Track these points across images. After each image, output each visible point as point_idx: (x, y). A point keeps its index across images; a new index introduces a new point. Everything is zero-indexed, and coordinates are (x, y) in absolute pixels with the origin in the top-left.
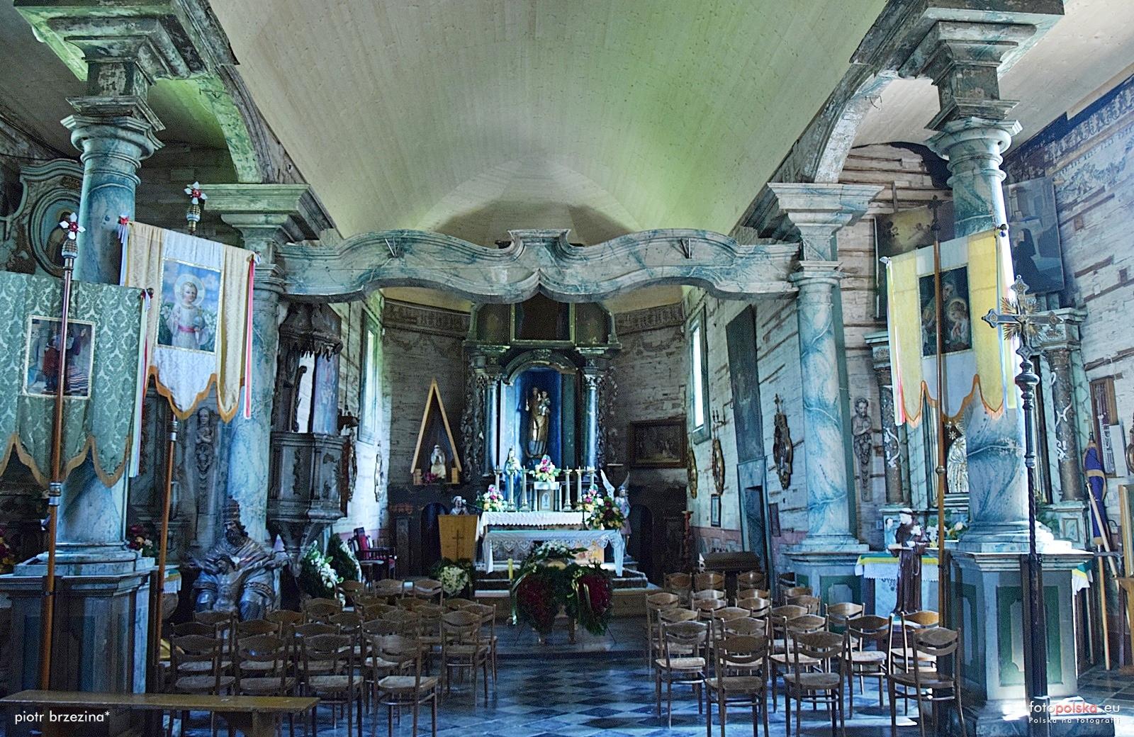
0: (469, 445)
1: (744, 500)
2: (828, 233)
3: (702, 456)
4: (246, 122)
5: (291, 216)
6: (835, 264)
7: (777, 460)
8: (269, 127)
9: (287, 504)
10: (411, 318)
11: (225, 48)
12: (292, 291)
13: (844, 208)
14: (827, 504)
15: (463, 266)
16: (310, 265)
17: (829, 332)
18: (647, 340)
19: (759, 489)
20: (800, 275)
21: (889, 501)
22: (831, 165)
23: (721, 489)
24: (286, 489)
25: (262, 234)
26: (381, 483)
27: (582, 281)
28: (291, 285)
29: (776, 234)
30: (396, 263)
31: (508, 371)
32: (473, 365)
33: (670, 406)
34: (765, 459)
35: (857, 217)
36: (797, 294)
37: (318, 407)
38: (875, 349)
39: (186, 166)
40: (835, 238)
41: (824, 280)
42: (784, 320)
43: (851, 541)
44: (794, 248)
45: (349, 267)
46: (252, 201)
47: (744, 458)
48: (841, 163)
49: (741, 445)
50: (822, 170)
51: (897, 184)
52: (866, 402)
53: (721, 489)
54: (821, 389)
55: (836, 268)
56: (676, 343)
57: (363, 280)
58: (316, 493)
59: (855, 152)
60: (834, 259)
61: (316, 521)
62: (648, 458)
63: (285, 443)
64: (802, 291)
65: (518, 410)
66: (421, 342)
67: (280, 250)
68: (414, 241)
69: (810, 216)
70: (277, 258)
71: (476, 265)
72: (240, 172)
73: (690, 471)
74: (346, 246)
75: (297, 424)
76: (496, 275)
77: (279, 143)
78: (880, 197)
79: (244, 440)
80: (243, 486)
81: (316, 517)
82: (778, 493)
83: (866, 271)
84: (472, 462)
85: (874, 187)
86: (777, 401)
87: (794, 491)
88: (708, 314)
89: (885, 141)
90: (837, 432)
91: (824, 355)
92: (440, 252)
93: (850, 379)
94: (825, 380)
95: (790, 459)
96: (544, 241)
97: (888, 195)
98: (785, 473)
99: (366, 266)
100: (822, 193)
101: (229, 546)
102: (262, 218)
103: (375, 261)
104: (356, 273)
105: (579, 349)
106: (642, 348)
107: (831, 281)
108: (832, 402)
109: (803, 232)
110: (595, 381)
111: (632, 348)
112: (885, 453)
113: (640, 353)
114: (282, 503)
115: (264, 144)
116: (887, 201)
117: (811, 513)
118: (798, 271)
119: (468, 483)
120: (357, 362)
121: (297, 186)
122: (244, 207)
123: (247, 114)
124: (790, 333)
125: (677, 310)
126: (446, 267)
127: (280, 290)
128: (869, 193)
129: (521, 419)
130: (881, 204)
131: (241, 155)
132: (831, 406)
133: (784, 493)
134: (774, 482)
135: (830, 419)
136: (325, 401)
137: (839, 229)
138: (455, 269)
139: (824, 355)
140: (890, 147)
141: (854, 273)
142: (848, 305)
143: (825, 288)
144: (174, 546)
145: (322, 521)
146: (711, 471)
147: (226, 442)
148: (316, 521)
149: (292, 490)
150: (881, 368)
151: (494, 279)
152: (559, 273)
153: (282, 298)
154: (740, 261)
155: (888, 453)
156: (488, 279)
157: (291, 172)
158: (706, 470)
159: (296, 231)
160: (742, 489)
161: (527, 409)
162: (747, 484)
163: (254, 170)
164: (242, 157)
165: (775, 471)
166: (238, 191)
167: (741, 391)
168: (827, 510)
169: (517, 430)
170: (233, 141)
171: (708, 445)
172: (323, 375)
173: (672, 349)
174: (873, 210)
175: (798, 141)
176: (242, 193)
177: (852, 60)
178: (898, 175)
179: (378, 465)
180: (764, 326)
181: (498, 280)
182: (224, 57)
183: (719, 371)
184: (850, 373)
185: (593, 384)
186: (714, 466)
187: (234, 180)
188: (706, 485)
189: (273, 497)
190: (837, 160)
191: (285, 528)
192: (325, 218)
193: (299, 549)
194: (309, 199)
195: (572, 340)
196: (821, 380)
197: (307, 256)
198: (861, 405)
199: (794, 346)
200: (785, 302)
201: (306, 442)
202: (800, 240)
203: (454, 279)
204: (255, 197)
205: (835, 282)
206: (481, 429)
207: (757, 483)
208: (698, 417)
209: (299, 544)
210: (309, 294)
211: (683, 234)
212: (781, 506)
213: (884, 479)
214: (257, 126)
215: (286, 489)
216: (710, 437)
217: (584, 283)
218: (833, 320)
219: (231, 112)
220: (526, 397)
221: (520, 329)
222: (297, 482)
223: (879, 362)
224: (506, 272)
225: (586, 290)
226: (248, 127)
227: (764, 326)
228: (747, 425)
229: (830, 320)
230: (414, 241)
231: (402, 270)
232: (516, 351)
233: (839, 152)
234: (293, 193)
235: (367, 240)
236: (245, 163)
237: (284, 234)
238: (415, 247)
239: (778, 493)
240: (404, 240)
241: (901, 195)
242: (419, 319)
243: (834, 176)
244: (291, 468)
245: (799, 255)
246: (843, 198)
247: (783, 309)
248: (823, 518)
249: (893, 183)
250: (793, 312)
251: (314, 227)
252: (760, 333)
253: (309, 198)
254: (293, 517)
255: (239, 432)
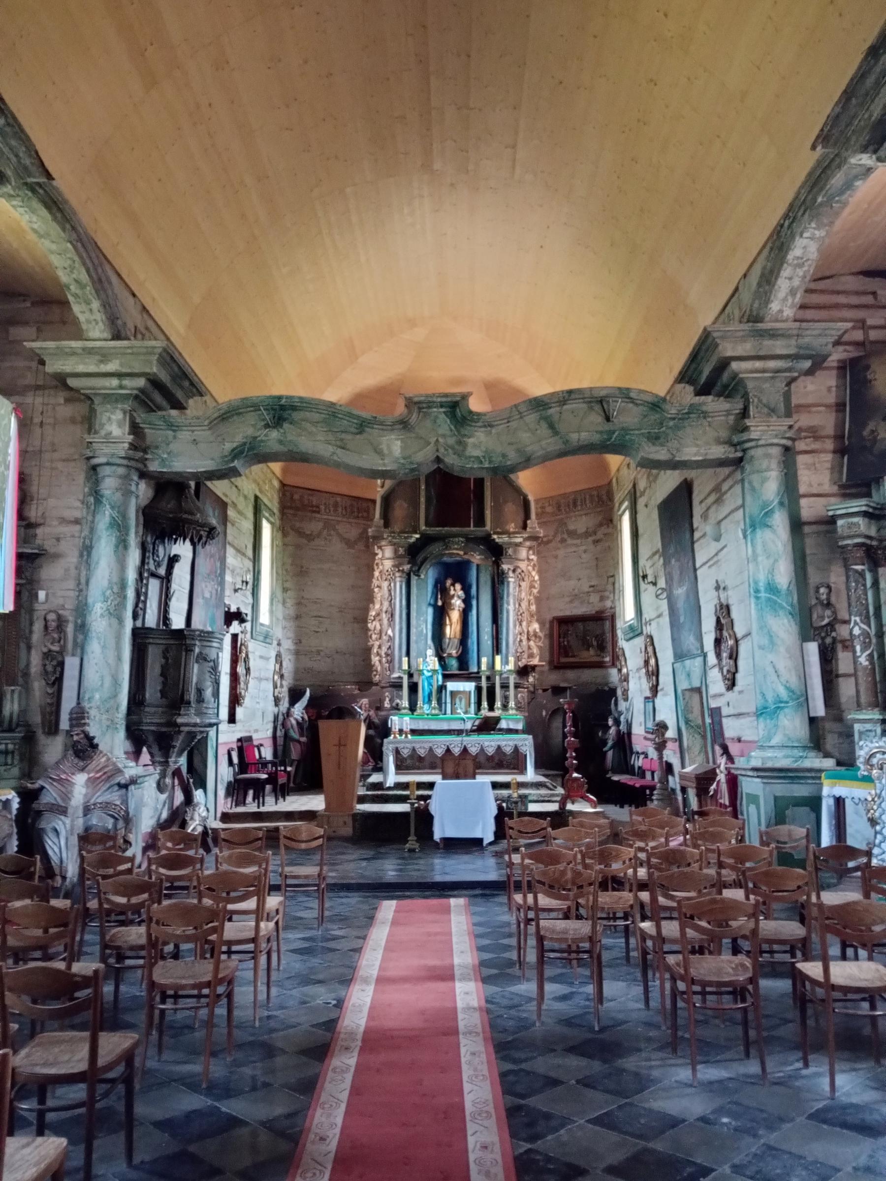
0: (377, 643)
1: (681, 702)
2: (781, 385)
3: (632, 652)
4: (84, 264)
5: (149, 380)
6: (789, 422)
7: (718, 655)
8: (119, 275)
9: (153, 710)
10: (312, 506)
11: (30, 156)
12: (154, 467)
13: (802, 352)
14: (782, 708)
15: (349, 437)
16: (175, 437)
17: (781, 504)
18: (572, 527)
19: (698, 690)
20: (745, 436)
21: (859, 706)
22: (785, 299)
23: (655, 690)
24: (152, 692)
25: (117, 401)
26: (282, 686)
27: (486, 452)
28: (152, 460)
29: (718, 388)
30: (274, 434)
31: (419, 562)
32: (380, 556)
33: (598, 598)
34: (705, 656)
35: (818, 363)
36: (741, 460)
37: (198, 601)
38: (840, 522)
39: (26, 323)
40: (789, 391)
41: (776, 441)
42: (726, 492)
43: (812, 754)
44: (738, 406)
45: (220, 439)
46: (101, 362)
47: (680, 656)
48: (798, 296)
49: (675, 641)
50: (775, 306)
51: (870, 322)
52: (829, 587)
53: (655, 690)
54: (772, 571)
55: (791, 427)
56: (604, 530)
57: (236, 454)
58: (186, 697)
59: (813, 286)
60: (788, 414)
61: (186, 729)
62: (573, 656)
63: (151, 641)
64: (748, 456)
65: (430, 604)
66: (325, 532)
67: (138, 420)
68: (294, 408)
69: (758, 364)
70: (135, 429)
71: (365, 435)
72: (84, 327)
73: (620, 670)
74: (216, 415)
75: (169, 619)
76: (389, 447)
77: (134, 295)
78: (846, 338)
79: (98, 638)
80: (97, 690)
81: (187, 725)
82: (721, 695)
83: (830, 430)
84: (380, 661)
85: (840, 324)
86: (717, 588)
87: (741, 692)
88: (638, 494)
89: (854, 270)
90: (793, 623)
91: (774, 532)
92: (324, 421)
93: (808, 559)
94: (776, 561)
95: (734, 656)
96: (442, 406)
97: (858, 335)
98: (728, 671)
99: (239, 439)
100: (773, 334)
101: (76, 760)
102: (115, 382)
103: (250, 431)
104: (228, 446)
105: (495, 537)
106: (565, 536)
107: (784, 442)
108: (785, 587)
109: (750, 385)
110: (514, 571)
111: (554, 536)
112: (854, 648)
113: (563, 541)
114: (147, 709)
115: (110, 292)
116: (857, 344)
117: (761, 719)
118: (742, 432)
119: (377, 684)
120: (250, 553)
121: (153, 343)
122: (92, 369)
123: (84, 255)
124: (733, 507)
125: (604, 492)
126: (330, 437)
127: (140, 466)
128: (833, 332)
129: (434, 613)
130: (847, 347)
131: (83, 305)
132: (783, 592)
133: (731, 696)
134: (716, 683)
135: (782, 608)
136: (207, 595)
137: (794, 379)
138: (342, 440)
139: (774, 532)
140: (861, 277)
141: (814, 433)
142: (806, 472)
143: (776, 451)
144: (16, 762)
145: (193, 729)
146: (644, 670)
147: (79, 640)
148: (186, 729)
149: (159, 695)
150: (848, 545)
151: (386, 451)
152: (460, 443)
153: (143, 475)
154: (671, 423)
155: (858, 648)
156: (379, 452)
157: (148, 326)
158: (638, 670)
159: (158, 398)
160: (679, 691)
161: (440, 603)
162: (683, 685)
163: (101, 324)
164: (84, 307)
165: (716, 670)
166: (84, 349)
167: (676, 577)
168: (781, 717)
169: (430, 626)
170: (72, 287)
171: (639, 642)
172: (203, 566)
173: (599, 535)
174: (837, 355)
175: (745, 276)
176: (90, 351)
177: (814, 147)
178: (871, 311)
179: (278, 666)
180: (701, 502)
181: (390, 452)
182: (33, 169)
183: (651, 557)
184: (808, 552)
185: (511, 574)
186: (647, 663)
187: (79, 335)
188: (638, 686)
189: (136, 701)
190: (793, 292)
191: (151, 738)
192: (192, 384)
193: (167, 762)
194: (168, 359)
195: (488, 527)
196: (771, 561)
197: (173, 427)
198: (822, 590)
199: (738, 522)
200: (727, 470)
201: (176, 639)
202: (746, 397)
203: (339, 451)
204: (104, 356)
205: (789, 443)
206: (390, 625)
207: (696, 683)
208: (628, 612)
209: (167, 755)
210: (174, 470)
211: (603, 393)
212: (725, 711)
213: (853, 679)
214: (100, 270)
215: (152, 692)
216: (641, 633)
217: (488, 454)
218: (787, 487)
219: (66, 250)
220: (441, 589)
221: (431, 516)
222: (164, 684)
223: (844, 538)
224: (399, 443)
225: (490, 462)
226: (88, 271)
227: (701, 502)
228: (685, 616)
229: (783, 489)
230: (294, 408)
231: (281, 442)
232: (427, 540)
233: (796, 282)
234: (150, 352)
235: (238, 408)
236: (88, 314)
237: (142, 400)
238: (296, 416)
239: (721, 695)
240: (283, 408)
241: (874, 335)
242: (322, 507)
243: (788, 312)
244: (157, 670)
245: (744, 413)
246: (801, 341)
247: (724, 480)
248: (776, 726)
249: (863, 322)
250: (736, 483)
251: (179, 395)
252: (697, 510)
253: (170, 358)
254: (158, 724)
255: (93, 628)
